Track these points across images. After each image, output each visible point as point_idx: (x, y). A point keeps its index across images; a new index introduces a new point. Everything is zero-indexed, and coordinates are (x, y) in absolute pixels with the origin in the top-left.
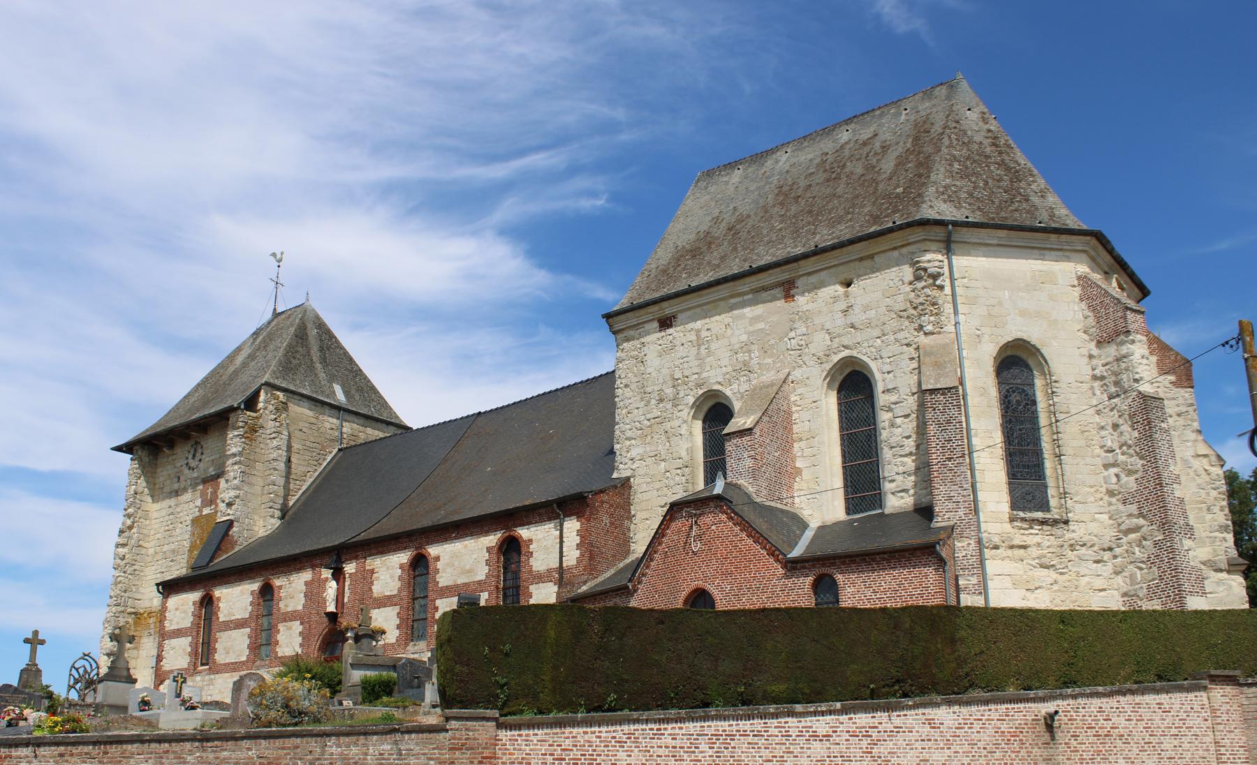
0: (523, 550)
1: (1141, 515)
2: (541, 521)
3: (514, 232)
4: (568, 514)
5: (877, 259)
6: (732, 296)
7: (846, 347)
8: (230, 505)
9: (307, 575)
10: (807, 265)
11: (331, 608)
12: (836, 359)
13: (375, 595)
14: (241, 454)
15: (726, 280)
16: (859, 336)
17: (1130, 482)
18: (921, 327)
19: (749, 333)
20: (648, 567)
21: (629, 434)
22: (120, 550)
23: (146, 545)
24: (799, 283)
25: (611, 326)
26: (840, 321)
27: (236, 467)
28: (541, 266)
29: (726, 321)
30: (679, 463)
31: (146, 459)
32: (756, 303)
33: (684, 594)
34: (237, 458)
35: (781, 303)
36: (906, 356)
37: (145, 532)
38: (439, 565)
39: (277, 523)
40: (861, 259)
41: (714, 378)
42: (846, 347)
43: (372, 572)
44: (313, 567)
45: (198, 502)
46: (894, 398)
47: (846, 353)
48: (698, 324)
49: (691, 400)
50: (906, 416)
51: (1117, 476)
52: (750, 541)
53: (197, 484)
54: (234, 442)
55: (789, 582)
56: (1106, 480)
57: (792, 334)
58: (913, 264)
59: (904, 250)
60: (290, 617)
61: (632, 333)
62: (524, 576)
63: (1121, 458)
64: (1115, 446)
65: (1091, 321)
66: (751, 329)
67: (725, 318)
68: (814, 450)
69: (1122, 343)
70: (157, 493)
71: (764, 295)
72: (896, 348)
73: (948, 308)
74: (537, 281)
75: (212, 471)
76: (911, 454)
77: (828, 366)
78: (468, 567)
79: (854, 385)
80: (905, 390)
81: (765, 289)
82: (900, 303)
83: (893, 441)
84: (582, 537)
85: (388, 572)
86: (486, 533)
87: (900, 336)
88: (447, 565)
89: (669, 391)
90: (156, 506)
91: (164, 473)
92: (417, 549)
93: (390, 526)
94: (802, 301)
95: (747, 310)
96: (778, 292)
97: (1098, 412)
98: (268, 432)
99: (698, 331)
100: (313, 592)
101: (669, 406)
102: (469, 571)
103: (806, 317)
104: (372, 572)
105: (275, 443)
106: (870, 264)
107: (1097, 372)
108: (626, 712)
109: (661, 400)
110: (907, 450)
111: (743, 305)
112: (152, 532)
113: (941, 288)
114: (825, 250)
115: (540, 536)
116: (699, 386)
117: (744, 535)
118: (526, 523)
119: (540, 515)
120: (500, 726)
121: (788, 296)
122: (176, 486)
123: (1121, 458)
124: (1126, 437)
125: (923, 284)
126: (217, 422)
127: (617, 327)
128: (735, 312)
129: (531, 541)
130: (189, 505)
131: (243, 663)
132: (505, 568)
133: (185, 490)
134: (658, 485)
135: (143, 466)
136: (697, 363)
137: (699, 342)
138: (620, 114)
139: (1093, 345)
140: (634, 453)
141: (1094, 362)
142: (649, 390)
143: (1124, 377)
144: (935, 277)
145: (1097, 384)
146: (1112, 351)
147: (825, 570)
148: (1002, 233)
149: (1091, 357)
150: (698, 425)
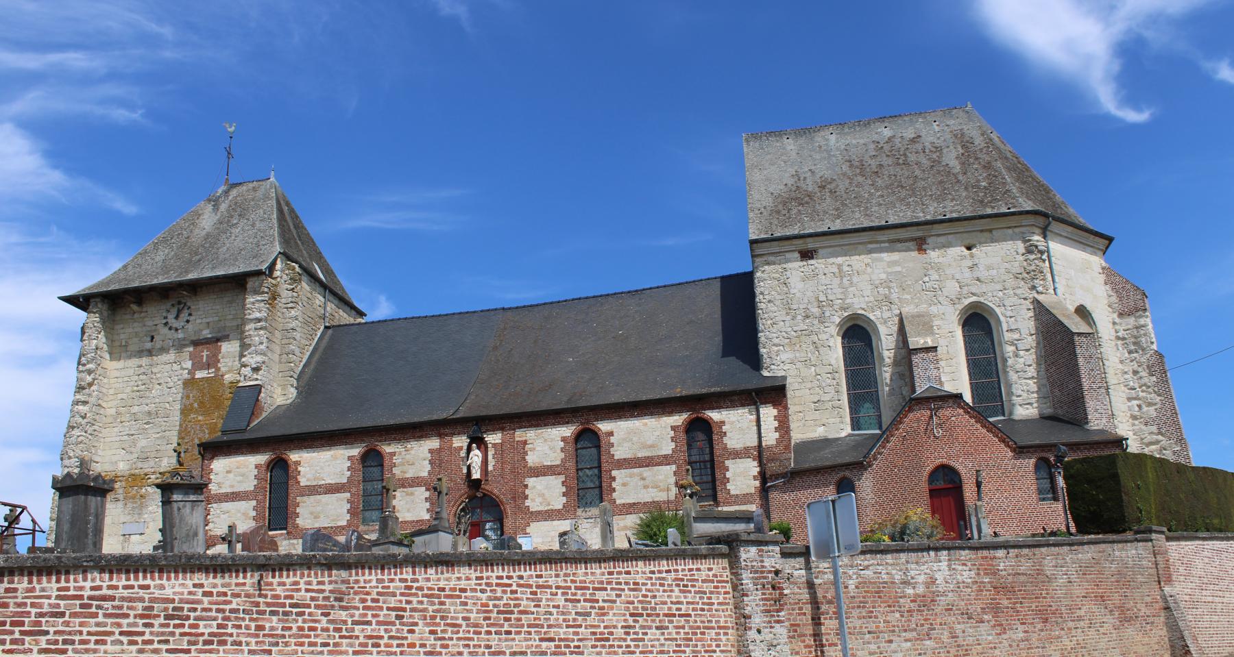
0: (715, 430)
1: (1160, 433)
2: (733, 405)
3: (34, 127)
4: (765, 402)
5: (994, 232)
6: (870, 243)
7: (973, 294)
8: (256, 370)
9: (434, 443)
11: (476, 475)
12: (967, 302)
13: (530, 464)
14: (266, 320)
15: (871, 229)
16: (984, 288)
17: (1152, 411)
18: (1034, 288)
19: (888, 274)
20: (884, 447)
21: (776, 341)
22: (81, 407)
23: (104, 404)
24: (929, 240)
25: (752, 250)
26: (967, 274)
27: (262, 332)
28: (55, 167)
30: (829, 369)
31: (105, 314)
32: (893, 251)
33: (929, 469)
34: (263, 324)
35: (915, 254)
36: (1025, 307)
37: (104, 391)
38: (612, 439)
39: (292, 393)
40: (982, 231)
41: (859, 304)
42: (973, 294)
43: (525, 443)
44: (503, 429)
45: (189, 364)
46: (1016, 336)
48: (840, 260)
49: (838, 320)
50: (1027, 350)
51: (1139, 406)
52: (984, 431)
53: (185, 346)
54: (255, 305)
55: (1018, 462)
56: (1130, 408)
57: (926, 279)
58: (1025, 241)
59: (1017, 230)
61: (771, 258)
63: (1141, 394)
64: (1136, 386)
65: (1114, 299)
66: (889, 270)
67: (866, 258)
68: (953, 369)
69: (1141, 317)
70: (118, 350)
71: (899, 245)
72: (1015, 300)
73: (1049, 276)
74: (53, 181)
75: (206, 333)
76: (1033, 378)
77: (960, 307)
78: (649, 443)
79: (978, 323)
80: (1025, 332)
81: (899, 241)
82: (1016, 268)
84: (780, 422)
85: (547, 444)
86: (670, 413)
87: (1019, 291)
88: (624, 440)
89: (815, 310)
90: (115, 364)
91: (130, 329)
93: (559, 400)
94: (933, 255)
95: (884, 255)
97: (1121, 362)
98: (284, 301)
99: (839, 266)
100: (437, 459)
101: (816, 322)
102: (652, 446)
103: (938, 268)
104: (525, 443)
105: (293, 312)
106: (990, 235)
107: (1120, 334)
109: (807, 317)
110: (1030, 375)
111: (881, 250)
112: (111, 392)
113: (1044, 261)
114: (951, 220)
116: (845, 309)
117: (979, 426)
118: (718, 407)
119: (731, 401)
120: (1168, 539)
121: (921, 249)
122: (149, 345)
123: (1141, 394)
124: (1146, 380)
125: (1033, 256)
126: (238, 283)
127: (758, 252)
128: (874, 255)
129: (723, 423)
130: (171, 371)
132: (690, 446)
133: (164, 350)
134: (809, 385)
135: (103, 321)
136: (840, 290)
137: (841, 274)
138: (167, 31)
139: (1115, 316)
140: (784, 357)
141: (1117, 327)
142: (794, 307)
143: (1143, 340)
144: (1042, 252)
145: (1119, 342)
146: (1131, 321)
147: (847, 474)
148: (1070, 229)
149: (1114, 323)
150: (839, 339)
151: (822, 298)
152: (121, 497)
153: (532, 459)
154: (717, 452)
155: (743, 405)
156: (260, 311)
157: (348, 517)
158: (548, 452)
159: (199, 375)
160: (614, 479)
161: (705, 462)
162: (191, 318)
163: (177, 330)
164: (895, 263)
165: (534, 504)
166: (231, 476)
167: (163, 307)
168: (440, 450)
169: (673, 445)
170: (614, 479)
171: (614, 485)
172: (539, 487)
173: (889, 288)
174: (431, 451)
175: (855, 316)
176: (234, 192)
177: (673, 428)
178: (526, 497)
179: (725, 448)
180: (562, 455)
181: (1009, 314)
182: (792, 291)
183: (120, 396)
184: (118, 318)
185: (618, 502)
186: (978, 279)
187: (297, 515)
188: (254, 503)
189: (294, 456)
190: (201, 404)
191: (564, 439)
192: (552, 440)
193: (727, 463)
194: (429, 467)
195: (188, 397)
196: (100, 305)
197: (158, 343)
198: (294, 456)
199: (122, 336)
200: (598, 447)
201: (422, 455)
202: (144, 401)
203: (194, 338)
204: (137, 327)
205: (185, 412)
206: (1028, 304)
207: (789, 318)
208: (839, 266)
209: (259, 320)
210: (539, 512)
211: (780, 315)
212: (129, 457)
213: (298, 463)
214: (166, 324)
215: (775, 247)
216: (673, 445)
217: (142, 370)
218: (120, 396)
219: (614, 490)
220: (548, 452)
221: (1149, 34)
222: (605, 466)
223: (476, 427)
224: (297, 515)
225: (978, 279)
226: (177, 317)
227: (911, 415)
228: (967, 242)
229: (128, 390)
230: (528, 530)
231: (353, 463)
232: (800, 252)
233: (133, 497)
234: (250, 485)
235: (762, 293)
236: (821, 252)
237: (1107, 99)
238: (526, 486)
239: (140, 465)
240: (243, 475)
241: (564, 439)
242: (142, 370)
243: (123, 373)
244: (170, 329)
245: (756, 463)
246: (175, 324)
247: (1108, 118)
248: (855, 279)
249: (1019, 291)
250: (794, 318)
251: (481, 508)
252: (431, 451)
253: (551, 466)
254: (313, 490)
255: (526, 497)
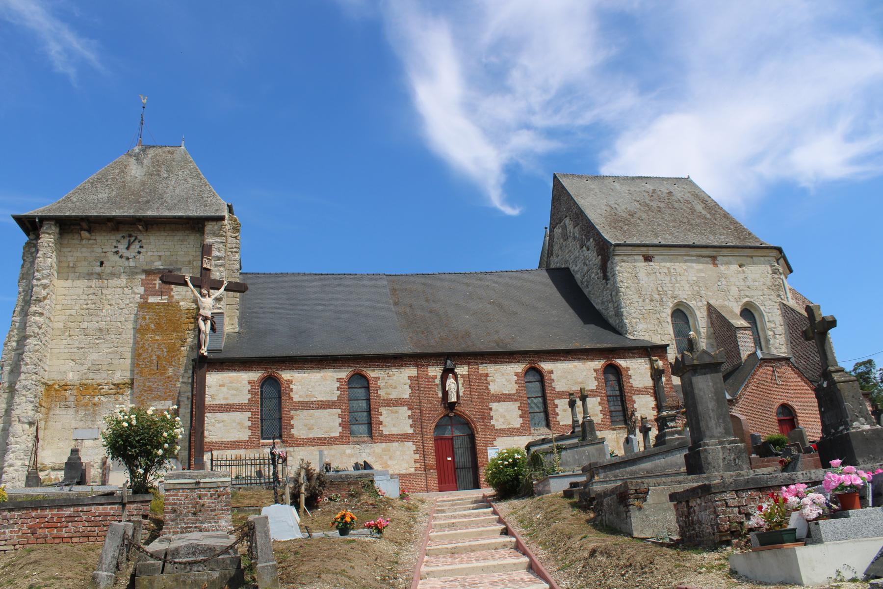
0: (624, 374)
2: (634, 356)
9: (412, 371)
10: (725, 252)
11: (453, 399)
18: (779, 296)
19: (698, 277)
21: (634, 315)
24: (719, 258)
27: (222, 269)
29: (685, 267)
31: (57, 236)
32: (699, 262)
35: (711, 266)
38: (553, 376)
43: (487, 375)
44: (469, 364)
45: (141, 290)
46: (773, 325)
47: (747, 299)
48: (668, 265)
49: (671, 305)
53: (137, 273)
59: (766, 258)
60: (640, 392)
61: (625, 258)
62: (257, 409)
67: (684, 266)
71: (702, 259)
77: (741, 304)
78: (580, 380)
81: (702, 256)
83: (777, 345)
85: (504, 377)
87: (772, 297)
89: (657, 297)
92: (529, 363)
95: (694, 265)
96: (709, 260)
99: (668, 269)
100: (416, 384)
102: (581, 383)
104: (487, 375)
108: (361, 530)
109: (652, 301)
110: (783, 350)
111: (692, 261)
112: (59, 307)
114: (729, 247)
115: (635, 366)
116: (675, 298)
119: (633, 354)
121: (715, 264)
129: (628, 368)
131: (336, 438)
133: (113, 275)
136: (670, 285)
151: (660, 289)
152: (72, 404)
153: (493, 388)
154: (627, 389)
155: (640, 357)
156: (219, 251)
157: (340, 429)
158: (505, 383)
159: (152, 300)
160: (556, 406)
161: (616, 396)
162: (142, 250)
163: (128, 259)
164: (701, 271)
165: (498, 423)
166: (224, 389)
167: (113, 237)
168: (418, 377)
169: (596, 383)
170: (556, 406)
171: (557, 410)
172: (501, 410)
173: (699, 287)
174: (410, 378)
175: (680, 303)
176: (151, 153)
177: (595, 370)
178: (492, 418)
179: (632, 387)
180: (517, 387)
181: (768, 311)
182: (641, 282)
183: (68, 312)
184: (66, 242)
185: (561, 423)
186: (748, 287)
187: (292, 426)
188: (249, 414)
189: (285, 375)
190: (158, 325)
191: (517, 374)
192: (508, 374)
193: (634, 397)
194: (409, 391)
195: (144, 318)
196: (53, 228)
197: (107, 268)
198: (285, 375)
199: (70, 259)
200: (367, 388)
201: (402, 381)
202: (96, 319)
203: (146, 268)
204: (86, 252)
205: (140, 331)
206: (777, 306)
207: (640, 300)
208: (668, 269)
209: (219, 258)
210: (503, 430)
211: (635, 298)
212: (78, 368)
213: (290, 382)
214: (117, 252)
215: (629, 251)
216: (596, 383)
217: (92, 291)
218: (68, 312)
219: (557, 414)
220: (505, 383)
221: (521, 161)
222: (549, 396)
223: (448, 359)
224: (292, 426)
225: (748, 287)
226: (128, 248)
227: (761, 370)
228: (740, 262)
229: (77, 307)
230: (495, 443)
231: (341, 384)
232: (644, 256)
233: (86, 405)
234: (244, 398)
235: (622, 281)
236: (656, 258)
237: (495, 198)
238: (491, 409)
239: (91, 376)
240: (236, 389)
241: (517, 374)
242: (92, 291)
243: (71, 291)
244: (121, 257)
245: (652, 399)
246: (126, 254)
247: (496, 210)
248: (679, 279)
249: (772, 297)
250: (644, 301)
251: (452, 425)
252: (410, 378)
253: (509, 394)
254: (306, 406)
255: (492, 418)
